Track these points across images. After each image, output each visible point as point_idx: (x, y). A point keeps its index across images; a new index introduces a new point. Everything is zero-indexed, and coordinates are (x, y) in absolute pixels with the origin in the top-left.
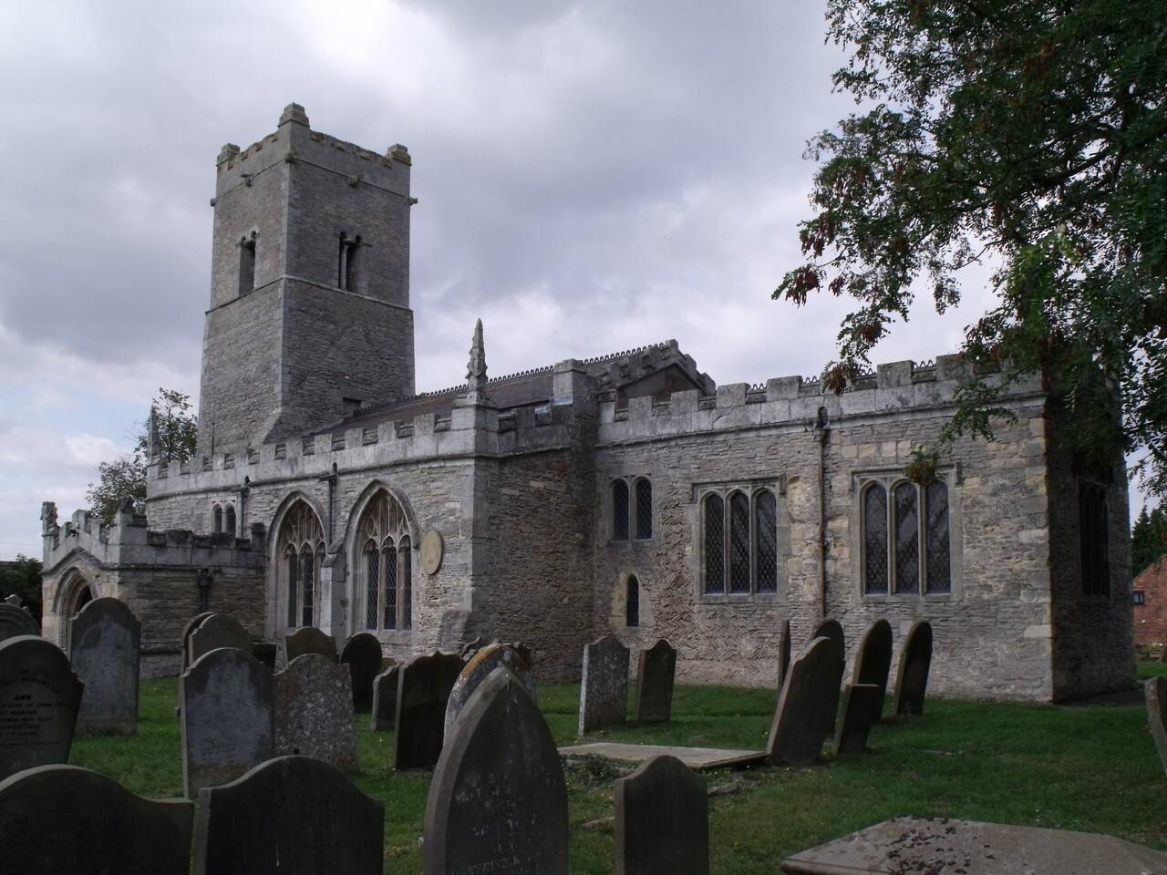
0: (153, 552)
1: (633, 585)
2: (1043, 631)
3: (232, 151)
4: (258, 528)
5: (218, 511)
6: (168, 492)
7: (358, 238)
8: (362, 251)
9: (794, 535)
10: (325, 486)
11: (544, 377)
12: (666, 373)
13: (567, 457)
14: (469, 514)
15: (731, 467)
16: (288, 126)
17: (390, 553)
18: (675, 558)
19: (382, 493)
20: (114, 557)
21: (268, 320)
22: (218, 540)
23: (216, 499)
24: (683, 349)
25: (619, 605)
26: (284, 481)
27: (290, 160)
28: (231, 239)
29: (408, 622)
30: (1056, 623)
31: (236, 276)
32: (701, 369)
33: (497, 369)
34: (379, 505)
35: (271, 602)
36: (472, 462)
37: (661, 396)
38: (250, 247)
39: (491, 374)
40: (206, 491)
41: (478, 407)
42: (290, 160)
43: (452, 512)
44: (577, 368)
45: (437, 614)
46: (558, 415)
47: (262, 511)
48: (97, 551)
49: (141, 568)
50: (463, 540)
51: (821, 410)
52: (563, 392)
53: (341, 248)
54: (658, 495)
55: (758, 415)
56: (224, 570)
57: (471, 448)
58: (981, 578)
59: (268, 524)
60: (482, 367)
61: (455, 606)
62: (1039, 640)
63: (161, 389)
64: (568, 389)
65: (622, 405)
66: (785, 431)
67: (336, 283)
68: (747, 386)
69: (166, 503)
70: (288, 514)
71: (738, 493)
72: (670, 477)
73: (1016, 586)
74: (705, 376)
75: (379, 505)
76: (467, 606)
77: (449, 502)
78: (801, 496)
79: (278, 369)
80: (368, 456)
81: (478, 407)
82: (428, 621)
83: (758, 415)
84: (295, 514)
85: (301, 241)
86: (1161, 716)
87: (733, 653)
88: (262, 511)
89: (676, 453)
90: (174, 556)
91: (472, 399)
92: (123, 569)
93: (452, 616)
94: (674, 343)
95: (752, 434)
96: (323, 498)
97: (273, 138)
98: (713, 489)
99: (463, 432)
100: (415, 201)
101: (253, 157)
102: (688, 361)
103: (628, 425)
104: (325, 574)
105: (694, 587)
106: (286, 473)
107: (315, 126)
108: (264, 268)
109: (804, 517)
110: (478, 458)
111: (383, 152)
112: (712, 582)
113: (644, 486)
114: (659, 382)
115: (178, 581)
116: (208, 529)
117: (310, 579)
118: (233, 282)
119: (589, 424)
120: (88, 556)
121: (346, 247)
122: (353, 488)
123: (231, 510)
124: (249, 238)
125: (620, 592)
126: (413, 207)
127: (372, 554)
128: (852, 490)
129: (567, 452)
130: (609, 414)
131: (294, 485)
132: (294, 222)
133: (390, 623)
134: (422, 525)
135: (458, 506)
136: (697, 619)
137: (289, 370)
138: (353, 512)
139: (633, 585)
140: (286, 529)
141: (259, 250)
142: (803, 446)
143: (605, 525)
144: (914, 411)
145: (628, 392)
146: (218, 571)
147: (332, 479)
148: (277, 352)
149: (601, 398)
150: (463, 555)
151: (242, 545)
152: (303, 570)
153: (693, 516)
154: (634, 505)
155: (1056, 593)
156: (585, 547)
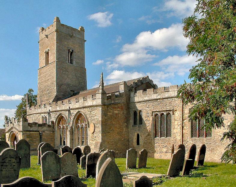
0: (29, 127)
1: (138, 135)
8: (74, 54)
10: (67, 112)
14: (100, 119)
22: (44, 125)
25: (135, 140)
26: (58, 111)
34: (79, 116)
36: (181, 144)
44: (125, 83)
46: (121, 95)
47: (54, 118)
48: (18, 128)
52: (122, 89)
53: (69, 53)
59: (54, 121)
64: (123, 89)
75: (79, 116)
77: (96, 116)
80: (77, 105)
84: (60, 118)
96: (67, 115)
99: (98, 101)
106: (58, 109)
121: (70, 53)
122: (74, 112)
123: (46, 117)
139: (138, 135)
143: (132, 121)
148: (55, 79)
151: (49, 126)
156: (127, 127)
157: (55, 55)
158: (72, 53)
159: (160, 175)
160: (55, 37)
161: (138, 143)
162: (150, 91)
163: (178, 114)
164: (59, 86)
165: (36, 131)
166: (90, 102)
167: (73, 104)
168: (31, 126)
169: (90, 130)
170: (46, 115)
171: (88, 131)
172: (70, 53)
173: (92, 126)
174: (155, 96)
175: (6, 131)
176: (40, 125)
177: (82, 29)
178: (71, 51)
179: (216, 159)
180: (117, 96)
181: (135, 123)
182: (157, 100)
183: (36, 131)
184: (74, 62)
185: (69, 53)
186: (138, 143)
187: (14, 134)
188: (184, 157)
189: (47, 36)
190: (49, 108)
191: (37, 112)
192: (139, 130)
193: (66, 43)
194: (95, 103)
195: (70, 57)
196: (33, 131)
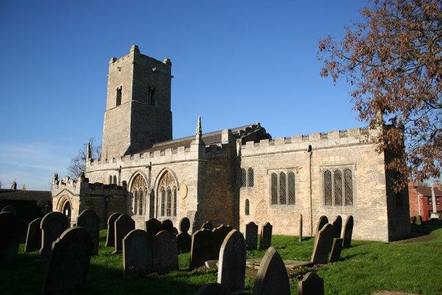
1: (247, 202)
4: (124, 182)
5: (111, 177)
18: (261, 193)
43: (191, 178)
51: (310, 147)
58: (363, 201)
59: (127, 183)
61: (191, 209)
73: (375, 203)
74: (263, 128)
80: (162, 159)
84: (136, 178)
90: (97, 191)
98: (274, 171)
106: (134, 164)
109: (304, 180)
112: (274, 201)
116: (107, 183)
122: (156, 170)
123: (115, 177)
127: (163, 192)
134: (180, 182)
136: (269, 213)
141: (122, 91)
158: (153, 91)
160: (132, 71)
162: (264, 142)
165: (100, 196)
166: (181, 154)
167: (158, 159)
176: (106, 186)
177: (169, 63)
183: (100, 196)
184: (156, 103)
190: (120, 163)
193: (146, 79)
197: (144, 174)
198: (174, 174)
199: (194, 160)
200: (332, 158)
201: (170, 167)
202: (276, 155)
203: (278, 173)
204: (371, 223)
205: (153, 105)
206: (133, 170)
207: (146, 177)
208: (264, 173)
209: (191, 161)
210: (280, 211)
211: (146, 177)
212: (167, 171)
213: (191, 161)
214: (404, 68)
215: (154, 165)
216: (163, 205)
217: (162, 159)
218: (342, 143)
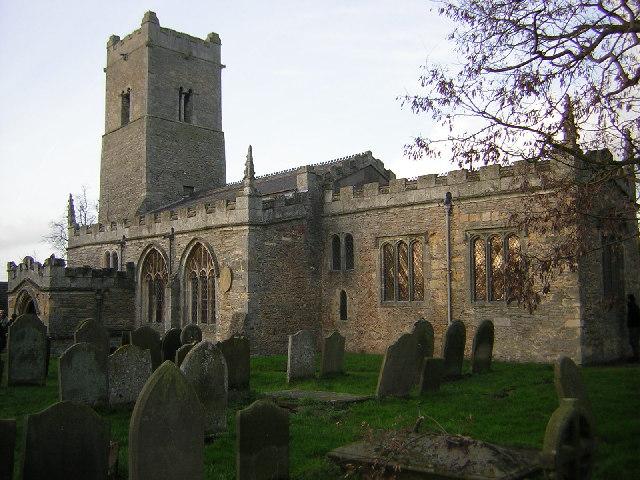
0: (68, 280)
1: (343, 295)
2: (576, 323)
3: (115, 39)
4: (130, 265)
5: (108, 255)
6: (79, 244)
7: (190, 91)
8: (193, 98)
9: (433, 267)
10: (167, 240)
11: (289, 177)
12: (366, 171)
13: (305, 222)
14: (246, 258)
15: (396, 228)
16: (147, 25)
17: (203, 277)
19: (199, 244)
20: (46, 284)
21: (138, 140)
22: (108, 272)
23: (107, 248)
24: (376, 156)
25: (336, 309)
26: (145, 238)
27: (148, 45)
28: (116, 92)
29: (214, 319)
30: (584, 318)
31: (120, 115)
32: (387, 167)
33: (259, 172)
34: (196, 252)
35: (138, 308)
36: (247, 228)
37: (359, 188)
38: (126, 97)
39: (259, 172)
40: (102, 243)
41: (250, 196)
42: (148, 45)
44: (310, 169)
45: (230, 315)
46: (299, 199)
47: (133, 254)
48: (37, 281)
49: (61, 290)
50: (242, 271)
51: (449, 194)
52: (303, 185)
53: (180, 96)
54: (357, 245)
55: (412, 197)
56: (111, 290)
57: (247, 219)
59: (136, 263)
60: (252, 172)
61: (238, 310)
62: (574, 329)
63: (435, 74)
64: (305, 184)
65: (337, 192)
66: (427, 206)
67: (177, 118)
68: (406, 180)
69: (79, 250)
70: (147, 256)
71: (401, 242)
72: (365, 232)
74: (389, 171)
75: (196, 252)
76: (245, 310)
77: (236, 249)
78: (437, 244)
79: (143, 169)
80: (192, 223)
81: (250, 196)
82: (224, 318)
83: (412, 197)
84: (151, 257)
85: (155, 91)
86: (406, 337)
87: (378, 329)
88: (133, 254)
89: (368, 219)
90: (81, 282)
91: (247, 190)
92: (51, 290)
93: (237, 316)
94: (370, 153)
95: (408, 209)
96: (166, 247)
97: (138, 32)
99: (242, 211)
100: (225, 67)
101: (126, 45)
102: (379, 163)
103: (342, 201)
104: (168, 293)
105: (377, 298)
106: (145, 233)
107: (163, 24)
108: (137, 109)
110: (250, 224)
111: (204, 37)
112: (387, 295)
113: (349, 238)
114: (361, 176)
115: (93, 299)
116: (102, 265)
117: (161, 296)
118: (118, 117)
119: (318, 204)
120: (32, 282)
121: (183, 96)
122: (182, 242)
123: (115, 254)
124: (126, 92)
125: (337, 299)
126: (223, 70)
127: (194, 280)
128: (465, 241)
129: (313, 216)
130: (329, 197)
131: (150, 240)
132: (151, 82)
133: (204, 319)
134: (220, 263)
135: (240, 253)
137: (150, 171)
138: (183, 256)
139: (343, 295)
140: (146, 264)
141: (131, 98)
142: (436, 216)
143: (329, 262)
144: (499, 194)
145: (341, 183)
146: (107, 290)
147: (171, 237)
148: (143, 160)
149: (324, 187)
150: (242, 283)
151: (121, 275)
152: (156, 289)
153: (376, 255)
154: (344, 251)
155: (584, 301)
156: (316, 274)
157: (146, 102)
158: (187, 97)
159: (323, 350)
160: (146, 60)
161: (344, 315)
162: (371, 188)
163: (437, 244)
164: (154, 175)
165: (86, 290)
166: (221, 217)
167: (188, 222)
168: (73, 278)
169: (222, 284)
170: (115, 247)
171: (216, 285)
172: (183, 96)
173: (225, 272)
174: (383, 201)
175: (10, 289)
176: (97, 274)
177: (215, 39)
178: (186, 90)
179: (536, 353)
180: (289, 202)
181: (337, 265)
182: (388, 208)
183: (86, 290)
184: (194, 117)
185: (180, 96)
186: (344, 315)
187: (27, 298)
188: (462, 348)
189: (125, 57)
190: (124, 231)
191: (94, 241)
192: (346, 283)
193: (173, 73)
194: (232, 220)
195: (183, 104)
196: (80, 290)
197: (162, 250)
198: (211, 248)
199: (242, 224)
200: (486, 216)
201: (203, 235)
202: (391, 211)
203: (393, 241)
204: (552, 334)
205: (189, 122)
206: (145, 243)
207: (164, 254)
208: (370, 240)
209: (237, 225)
210: (398, 312)
211: (164, 254)
212: (199, 244)
213: (237, 225)
214: (554, 16)
215: (178, 233)
216: (195, 304)
217: (192, 223)
218: (504, 187)
